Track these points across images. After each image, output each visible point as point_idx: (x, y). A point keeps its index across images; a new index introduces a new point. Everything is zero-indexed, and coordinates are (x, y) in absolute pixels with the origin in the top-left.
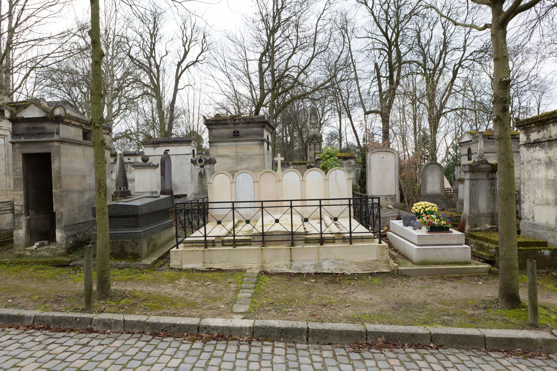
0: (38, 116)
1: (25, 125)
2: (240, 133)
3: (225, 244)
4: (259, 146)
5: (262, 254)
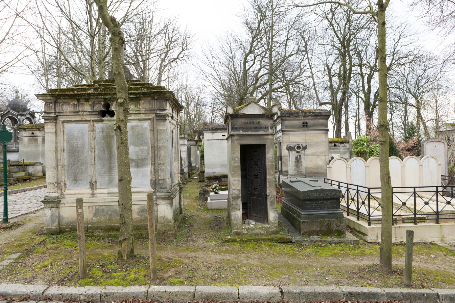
0: (258, 113)
1: (242, 121)
2: (309, 124)
3: (405, 221)
5: (441, 230)
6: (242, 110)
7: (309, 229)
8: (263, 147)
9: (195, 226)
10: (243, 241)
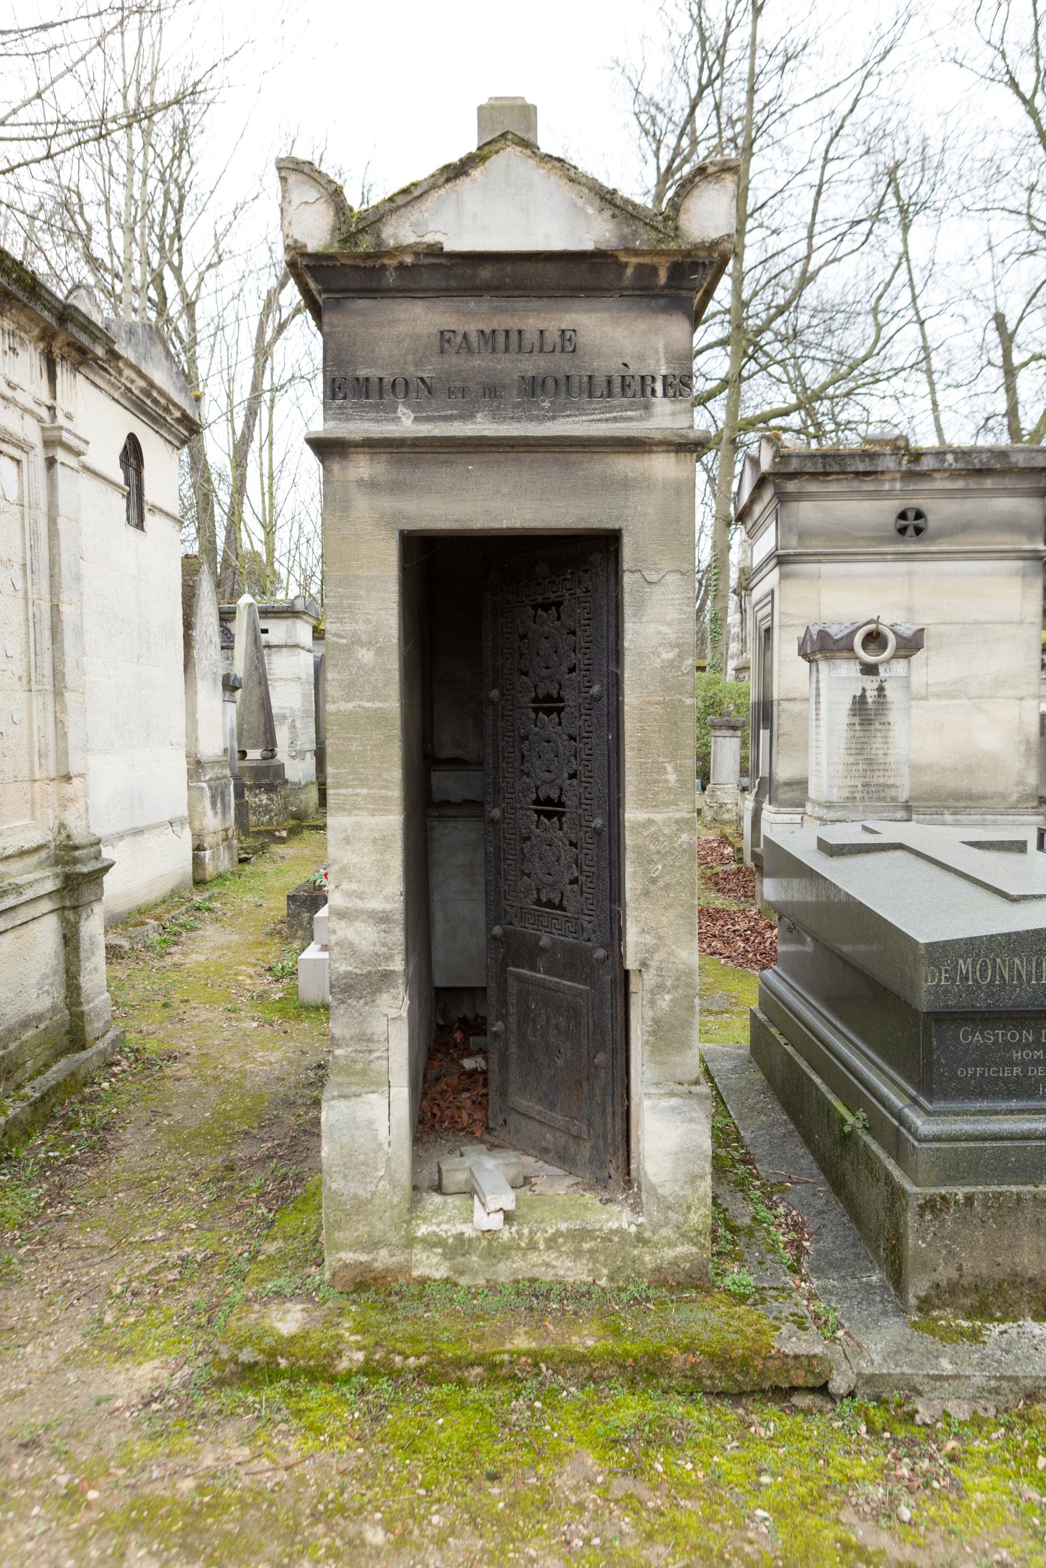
1: (417, 321)
2: (933, 521)
4: (1017, 582)
6: (414, 214)
7: (975, 1264)
8: (594, 553)
9: (132, 1151)
10: (395, 1375)
